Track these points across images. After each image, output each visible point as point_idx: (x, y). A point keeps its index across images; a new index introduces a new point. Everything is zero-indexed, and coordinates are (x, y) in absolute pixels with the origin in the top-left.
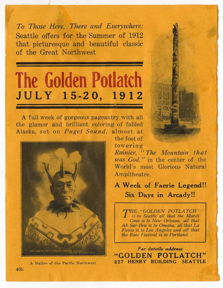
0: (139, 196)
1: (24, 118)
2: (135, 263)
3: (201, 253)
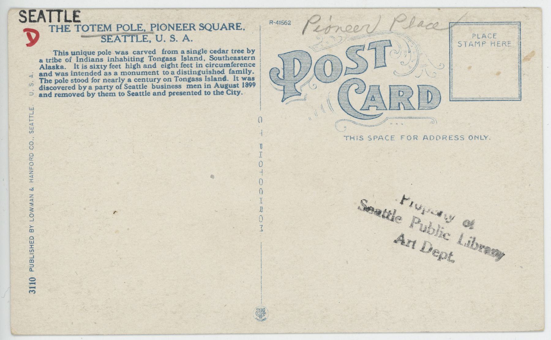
2: (181, 30)
3: (57, 31)
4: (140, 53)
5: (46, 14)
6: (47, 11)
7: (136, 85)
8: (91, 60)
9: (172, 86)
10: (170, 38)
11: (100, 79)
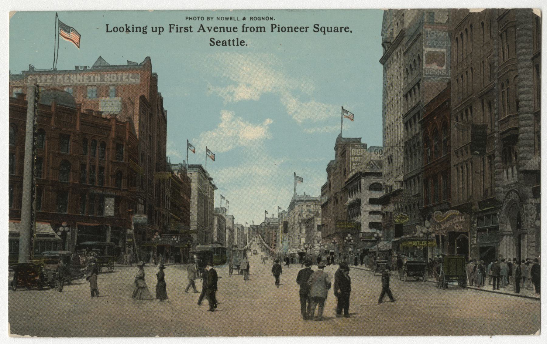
0: (107, 31)
1: (202, 30)
4: (339, 30)
7: (228, 40)
8: (333, 29)
9: (295, 28)
11: (308, 27)
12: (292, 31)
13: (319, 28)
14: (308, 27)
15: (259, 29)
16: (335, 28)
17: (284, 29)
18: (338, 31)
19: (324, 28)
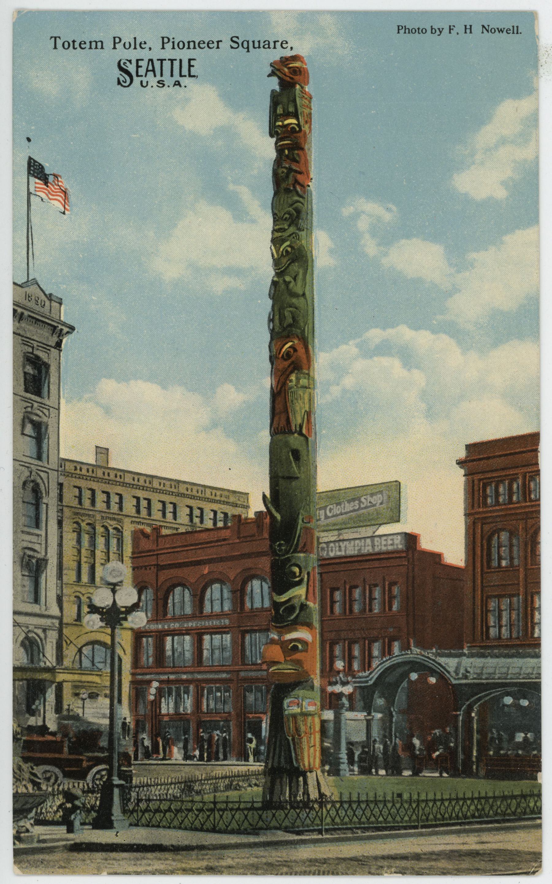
4: (272, 45)
5: (157, 65)
6: (158, 60)
9: (199, 43)
10: (117, 73)
11: (221, 41)
12: (194, 48)
13: (240, 42)
14: (221, 41)
15: (94, 45)
16: (264, 42)
17: (181, 45)
18: (269, 48)
19: (248, 42)
